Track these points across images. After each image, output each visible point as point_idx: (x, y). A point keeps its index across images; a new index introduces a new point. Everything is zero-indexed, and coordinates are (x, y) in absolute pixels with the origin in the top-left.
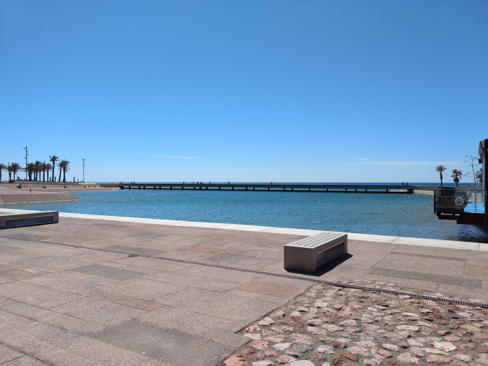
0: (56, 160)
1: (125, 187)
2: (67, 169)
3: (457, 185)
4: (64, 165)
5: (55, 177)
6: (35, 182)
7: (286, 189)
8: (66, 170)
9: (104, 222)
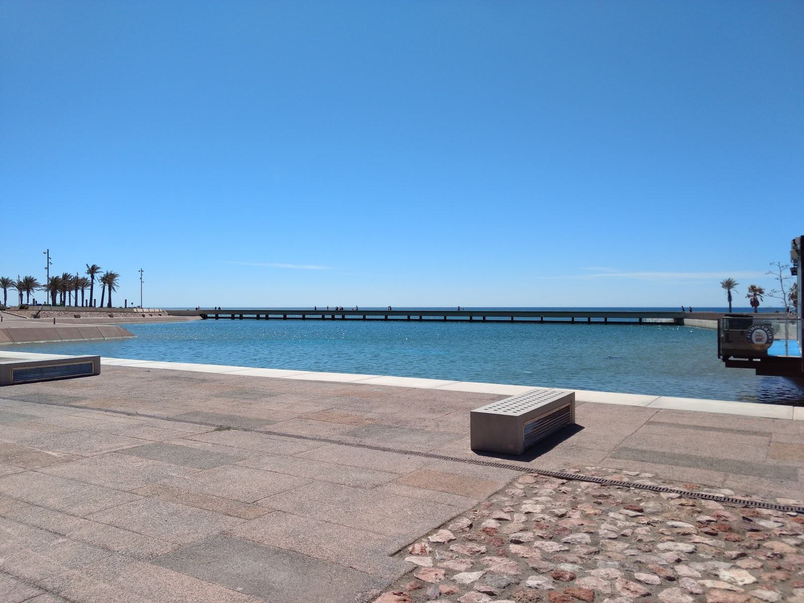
0: (97, 271)
2: (115, 287)
3: (756, 311)
4: (109, 280)
5: (95, 300)
9: (175, 374)
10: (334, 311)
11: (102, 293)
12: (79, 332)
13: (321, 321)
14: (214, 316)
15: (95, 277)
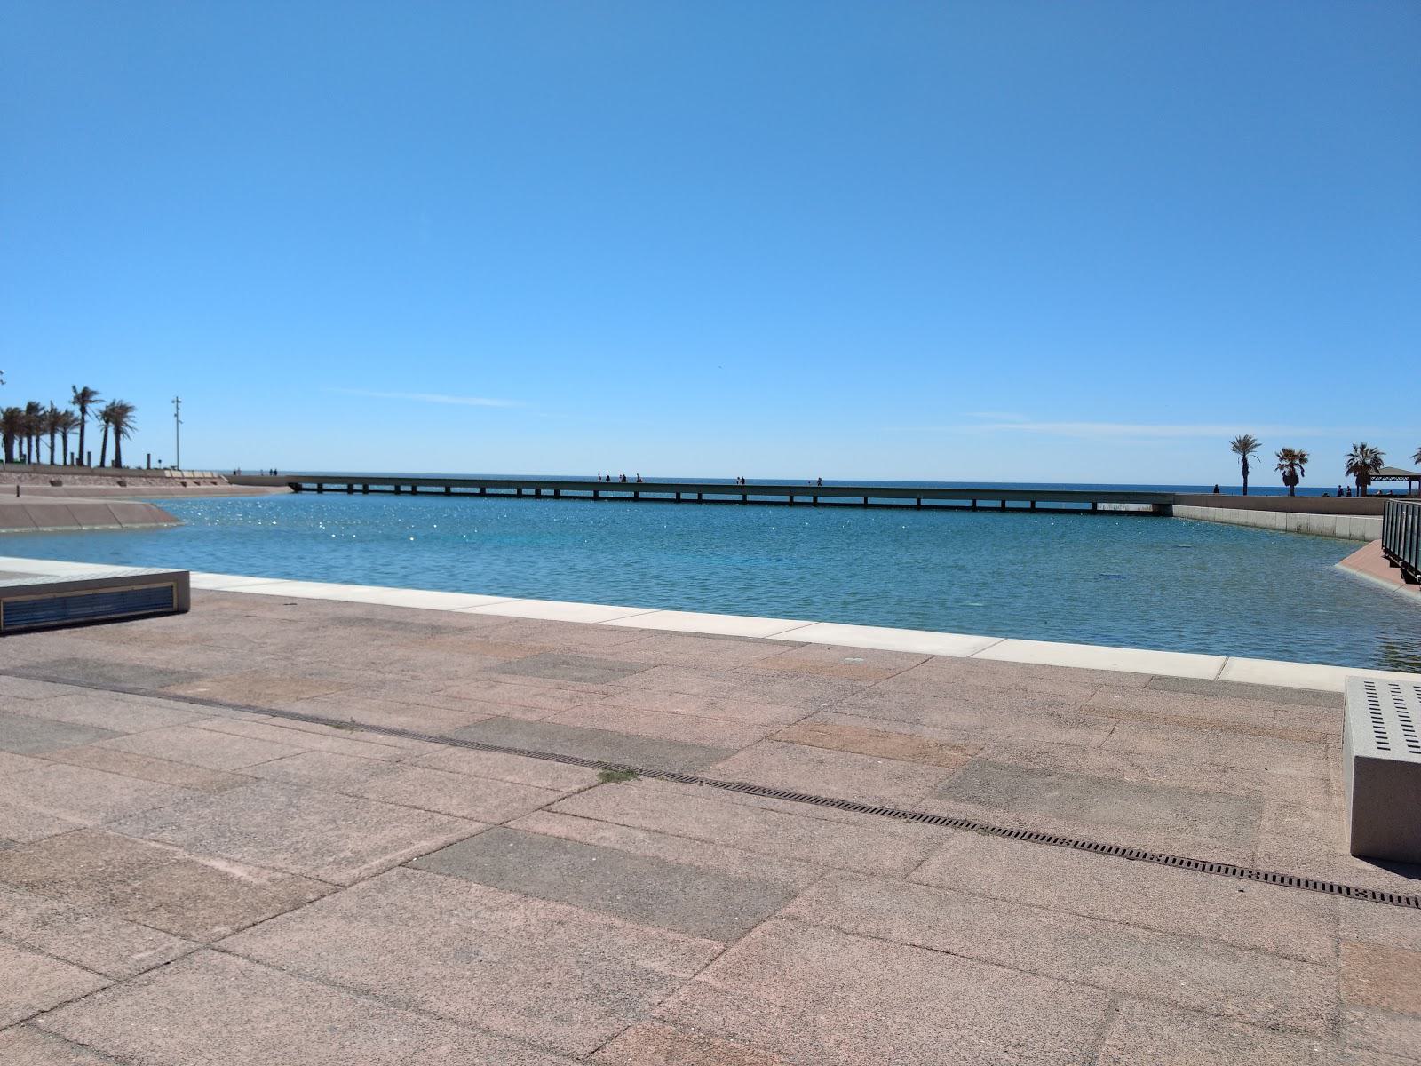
1: (305, 486)
2: (128, 430)
3: (1292, 494)
4: (116, 416)
5: (89, 454)
6: (25, 467)
7: (797, 499)
8: (123, 432)
9: (359, 612)
10: (619, 484)
11: (102, 441)
12: (71, 513)
13: (479, 498)
14: (315, 486)
15: (88, 410)
